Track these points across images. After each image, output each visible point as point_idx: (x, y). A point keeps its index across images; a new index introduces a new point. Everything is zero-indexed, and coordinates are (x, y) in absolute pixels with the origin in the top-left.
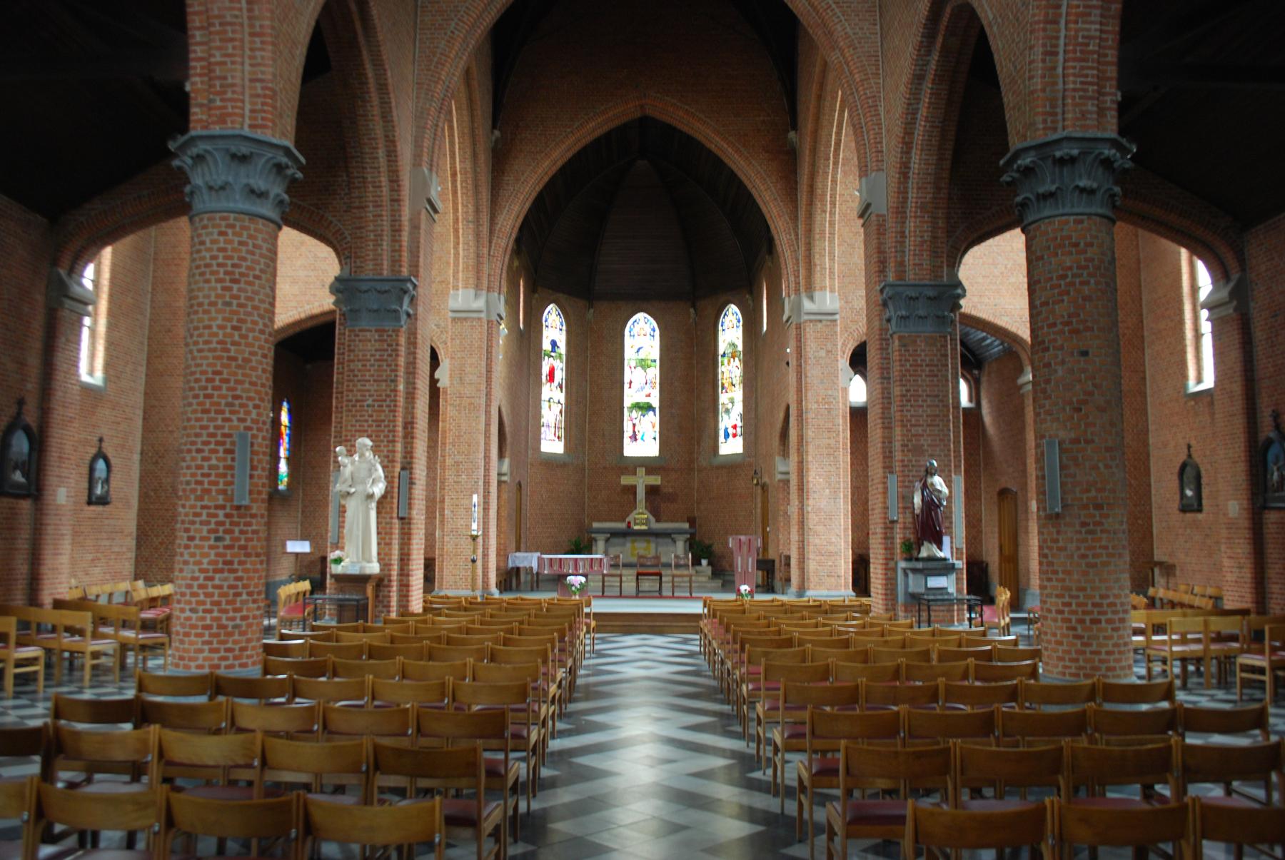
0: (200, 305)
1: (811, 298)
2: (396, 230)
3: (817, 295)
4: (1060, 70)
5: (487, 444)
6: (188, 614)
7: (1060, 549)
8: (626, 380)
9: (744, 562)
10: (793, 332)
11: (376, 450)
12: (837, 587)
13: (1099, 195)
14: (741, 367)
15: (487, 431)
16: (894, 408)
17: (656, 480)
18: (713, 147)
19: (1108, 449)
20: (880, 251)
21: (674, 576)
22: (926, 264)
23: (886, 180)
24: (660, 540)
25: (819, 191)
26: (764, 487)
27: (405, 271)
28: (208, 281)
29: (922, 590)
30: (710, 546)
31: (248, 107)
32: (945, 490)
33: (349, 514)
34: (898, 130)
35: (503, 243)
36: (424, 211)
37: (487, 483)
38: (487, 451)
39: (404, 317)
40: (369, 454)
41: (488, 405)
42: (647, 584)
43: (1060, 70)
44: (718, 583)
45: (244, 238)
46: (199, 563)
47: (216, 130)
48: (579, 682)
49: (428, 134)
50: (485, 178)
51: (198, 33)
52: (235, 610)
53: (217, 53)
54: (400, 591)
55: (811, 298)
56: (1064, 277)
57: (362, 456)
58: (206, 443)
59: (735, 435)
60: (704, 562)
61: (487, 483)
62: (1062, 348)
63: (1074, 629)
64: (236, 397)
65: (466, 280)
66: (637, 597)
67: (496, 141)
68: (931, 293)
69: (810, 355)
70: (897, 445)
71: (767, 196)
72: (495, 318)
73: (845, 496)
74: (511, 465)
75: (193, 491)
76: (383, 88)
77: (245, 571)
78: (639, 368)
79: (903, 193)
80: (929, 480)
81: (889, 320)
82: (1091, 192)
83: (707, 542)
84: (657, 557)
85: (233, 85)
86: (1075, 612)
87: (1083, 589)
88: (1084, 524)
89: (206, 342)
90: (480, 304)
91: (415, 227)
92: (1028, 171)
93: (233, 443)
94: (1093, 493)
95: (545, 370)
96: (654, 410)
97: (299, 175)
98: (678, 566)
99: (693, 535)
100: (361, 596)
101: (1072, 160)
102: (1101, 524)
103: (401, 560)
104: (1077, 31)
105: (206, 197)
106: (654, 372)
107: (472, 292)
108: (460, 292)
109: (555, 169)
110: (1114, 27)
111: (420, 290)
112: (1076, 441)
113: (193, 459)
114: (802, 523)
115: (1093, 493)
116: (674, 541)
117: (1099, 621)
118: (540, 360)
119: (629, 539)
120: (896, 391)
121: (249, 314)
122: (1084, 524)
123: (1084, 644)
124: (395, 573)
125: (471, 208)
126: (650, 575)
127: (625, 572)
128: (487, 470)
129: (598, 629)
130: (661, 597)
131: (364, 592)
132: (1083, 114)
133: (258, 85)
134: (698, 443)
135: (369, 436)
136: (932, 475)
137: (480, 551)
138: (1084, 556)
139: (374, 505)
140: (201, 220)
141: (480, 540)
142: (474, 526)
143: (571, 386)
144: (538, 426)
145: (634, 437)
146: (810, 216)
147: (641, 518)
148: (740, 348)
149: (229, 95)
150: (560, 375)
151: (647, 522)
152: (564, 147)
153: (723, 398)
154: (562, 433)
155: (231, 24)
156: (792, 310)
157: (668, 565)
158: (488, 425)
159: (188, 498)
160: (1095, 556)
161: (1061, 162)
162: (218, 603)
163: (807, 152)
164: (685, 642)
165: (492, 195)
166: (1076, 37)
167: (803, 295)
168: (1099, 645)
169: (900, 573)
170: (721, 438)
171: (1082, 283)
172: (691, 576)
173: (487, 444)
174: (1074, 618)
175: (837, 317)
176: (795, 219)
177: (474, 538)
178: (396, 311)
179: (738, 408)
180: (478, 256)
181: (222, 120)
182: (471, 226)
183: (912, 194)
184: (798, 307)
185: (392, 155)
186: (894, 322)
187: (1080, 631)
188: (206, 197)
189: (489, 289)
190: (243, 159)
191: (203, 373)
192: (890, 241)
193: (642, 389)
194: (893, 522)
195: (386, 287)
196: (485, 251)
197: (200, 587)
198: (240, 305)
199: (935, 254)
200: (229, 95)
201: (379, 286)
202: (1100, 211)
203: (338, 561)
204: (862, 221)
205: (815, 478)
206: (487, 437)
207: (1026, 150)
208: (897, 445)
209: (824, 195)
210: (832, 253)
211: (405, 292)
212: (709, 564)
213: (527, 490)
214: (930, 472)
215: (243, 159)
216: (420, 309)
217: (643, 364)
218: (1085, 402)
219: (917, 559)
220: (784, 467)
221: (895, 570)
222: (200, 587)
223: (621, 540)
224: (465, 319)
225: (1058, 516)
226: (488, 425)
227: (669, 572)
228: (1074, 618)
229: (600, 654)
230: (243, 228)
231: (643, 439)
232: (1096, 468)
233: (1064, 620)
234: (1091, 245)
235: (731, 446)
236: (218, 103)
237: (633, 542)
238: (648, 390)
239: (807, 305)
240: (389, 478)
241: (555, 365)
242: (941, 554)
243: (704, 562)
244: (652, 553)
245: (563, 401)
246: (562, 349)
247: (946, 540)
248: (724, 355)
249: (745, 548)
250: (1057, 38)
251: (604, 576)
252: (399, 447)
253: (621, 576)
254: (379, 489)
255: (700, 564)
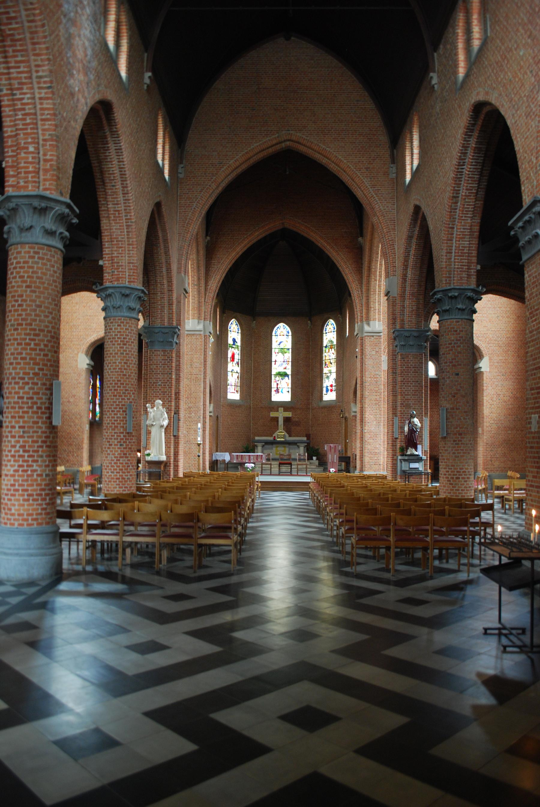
0: (111, 354)
1: (368, 324)
2: (171, 304)
3: (371, 323)
4: (453, 260)
5: (204, 398)
6: (110, 473)
7: (446, 450)
8: (273, 360)
9: (332, 457)
10: (359, 342)
11: (163, 405)
12: (378, 470)
13: (466, 311)
14: (335, 354)
15: (204, 391)
16: (398, 387)
17: (289, 414)
18: (319, 245)
19: (465, 412)
20: (393, 314)
21: (298, 465)
22: (414, 321)
23: (397, 280)
24: (291, 446)
25: (373, 270)
26: (346, 418)
27: (175, 323)
28: (114, 344)
29: (408, 469)
30: (318, 450)
31: (127, 274)
32: (419, 425)
33: (153, 434)
34: (402, 259)
35: (212, 295)
36: (182, 295)
37: (204, 417)
38: (204, 401)
39: (175, 344)
40: (161, 407)
41: (205, 378)
42: (284, 469)
43: (453, 260)
44: (322, 469)
45: (127, 327)
46: (114, 454)
47: (116, 284)
48: (255, 507)
49: (184, 258)
50: (202, 263)
51: (107, 244)
52: (128, 472)
53: (116, 253)
54: (174, 468)
55: (368, 324)
56: (450, 344)
57: (158, 408)
58: (116, 408)
59: (331, 390)
60: (314, 458)
61: (204, 417)
62: (449, 372)
63: (450, 481)
64: (126, 390)
65: (193, 315)
66: (279, 475)
67: (208, 242)
68: (415, 334)
69: (367, 353)
70: (399, 404)
71: (347, 271)
72: (208, 334)
73: (384, 425)
74: (214, 407)
75: (111, 427)
76: (166, 241)
77: (131, 457)
78: (280, 354)
79: (404, 288)
80: (412, 420)
81: (396, 346)
82: (463, 310)
83: (316, 448)
84: (290, 455)
85: (122, 266)
86: (450, 475)
87: (452, 466)
88: (454, 441)
89: (114, 369)
90: (200, 327)
91: (179, 302)
92: (439, 300)
93: (126, 408)
94: (458, 429)
95: (230, 355)
96: (288, 376)
97: (75, 221)
98: (300, 460)
99: (308, 444)
100: (158, 470)
101: (455, 297)
102: (461, 441)
103: (175, 454)
104: (459, 244)
105: (112, 311)
106: (288, 356)
107: (196, 321)
108: (191, 320)
109: (238, 256)
110: (475, 241)
111: (181, 332)
112: (453, 409)
113: (110, 414)
114: (362, 438)
115: (458, 429)
116: (299, 447)
117: (459, 478)
118: (227, 350)
119: (274, 446)
120: (399, 379)
121: (130, 357)
122: (454, 441)
123: (453, 487)
124: (172, 460)
125: (196, 278)
126: (285, 462)
127: (273, 463)
128: (204, 411)
129: (263, 488)
130: (291, 475)
131: (160, 468)
132: (461, 278)
133: (131, 265)
134: (312, 395)
135: (160, 399)
136: (414, 418)
137: (201, 451)
138: (454, 453)
139: (163, 430)
140: (110, 320)
141: (201, 446)
142: (199, 439)
143: (244, 363)
144: (226, 385)
145: (277, 391)
146: (368, 282)
147: (281, 434)
148: (335, 343)
149: (120, 270)
150: (237, 357)
151: (284, 437)
152: (243, 245)
153: (325, 370)
154: (239, 389)
155: (121, 241)
156: (359, 330)
157: (295, 460)
158: (205, 388)
159: (108, 429)
160: (458, 453)
161: (451, 298)
162: (122, 470)
163: (367, 250)
164: (303, 494)
165: (206, 271)
166: (459, 247)
167: (365, 322)
168: (459, 487)
169: (399, 461)
170: (324, 392)
171: (458, 347)
172: (306, 465)
173: (204, 398)
174: (450, 477)
175: (381, 334)
176: (361, 283)
177: (199, 445)
178: (171, 342)
179: (334, 376)
180: (199, 302)
181: (118, 279)
182: (196, 287)
183: (407, 289)
184: (362, 329)
185: (169, 270)
186: (398, 347)
187: (452, 482)
188: (112, 311)
189: (205, 319)
190: (127, 296)
191: (113, 381)
192: (398, 308)
193: (282, 364)
194: (396, 438)
195: (167, 330)
196: (203, 299)
197: (115, 463)
198: (127, 354)
199: (418, 315)
200: (120, 270)
201: (163, 330)
202: (466, 317)
203: (149, 455)
204: (386, 298)
205: (369, 416)
206: (204, 394)
207: (439, 291)
208: (399, 404)
209: (376, 272)
210: (379, 301)
211: (175, 333)
212: (317, 459)
213: (221, 419)
214: (412, 416)
215: (127, 296)
216: (181, 340)
217: (282, 351)
218: (457, 393)
219: (406, 455)
220: (355, 408)
221: (396, 460)
222: (115, 463)
223: (270, 446)
224: (193, 335)
225: (445, 437)
226: (205, 388)
227: (296, 463)
228: (450, 477)
229: (262, 498)
230: (127, 323)
231: (282, 392)
232: (460, 419)
233: (447, 478)
234: (462, 331)
235: (330, 396)
236: (116, 273)
237: (277, 447)
238: (285, 365)
239: (366, 328)
240: (169, 418)
241: (235, 352)
242: (417, 453)
243: (314, 458)
244: (287, 453)
245: (239, 371)
246: (239, 343)
247: (419, 447)
248: (326, 347)
249: (333, 450)
250: (452, 246)
251: (262, 464)
252: (173, 404)
253: (271, 464)
254: (166, 423)
255: (312, 459)
